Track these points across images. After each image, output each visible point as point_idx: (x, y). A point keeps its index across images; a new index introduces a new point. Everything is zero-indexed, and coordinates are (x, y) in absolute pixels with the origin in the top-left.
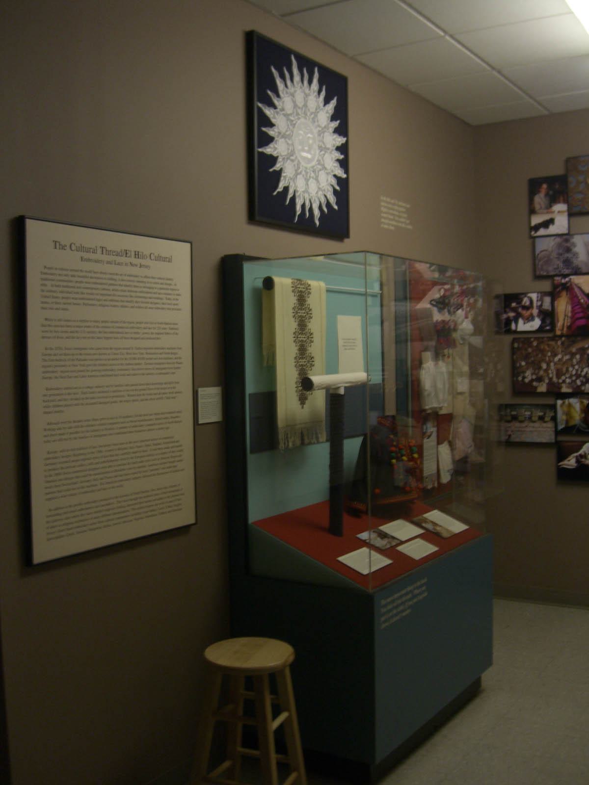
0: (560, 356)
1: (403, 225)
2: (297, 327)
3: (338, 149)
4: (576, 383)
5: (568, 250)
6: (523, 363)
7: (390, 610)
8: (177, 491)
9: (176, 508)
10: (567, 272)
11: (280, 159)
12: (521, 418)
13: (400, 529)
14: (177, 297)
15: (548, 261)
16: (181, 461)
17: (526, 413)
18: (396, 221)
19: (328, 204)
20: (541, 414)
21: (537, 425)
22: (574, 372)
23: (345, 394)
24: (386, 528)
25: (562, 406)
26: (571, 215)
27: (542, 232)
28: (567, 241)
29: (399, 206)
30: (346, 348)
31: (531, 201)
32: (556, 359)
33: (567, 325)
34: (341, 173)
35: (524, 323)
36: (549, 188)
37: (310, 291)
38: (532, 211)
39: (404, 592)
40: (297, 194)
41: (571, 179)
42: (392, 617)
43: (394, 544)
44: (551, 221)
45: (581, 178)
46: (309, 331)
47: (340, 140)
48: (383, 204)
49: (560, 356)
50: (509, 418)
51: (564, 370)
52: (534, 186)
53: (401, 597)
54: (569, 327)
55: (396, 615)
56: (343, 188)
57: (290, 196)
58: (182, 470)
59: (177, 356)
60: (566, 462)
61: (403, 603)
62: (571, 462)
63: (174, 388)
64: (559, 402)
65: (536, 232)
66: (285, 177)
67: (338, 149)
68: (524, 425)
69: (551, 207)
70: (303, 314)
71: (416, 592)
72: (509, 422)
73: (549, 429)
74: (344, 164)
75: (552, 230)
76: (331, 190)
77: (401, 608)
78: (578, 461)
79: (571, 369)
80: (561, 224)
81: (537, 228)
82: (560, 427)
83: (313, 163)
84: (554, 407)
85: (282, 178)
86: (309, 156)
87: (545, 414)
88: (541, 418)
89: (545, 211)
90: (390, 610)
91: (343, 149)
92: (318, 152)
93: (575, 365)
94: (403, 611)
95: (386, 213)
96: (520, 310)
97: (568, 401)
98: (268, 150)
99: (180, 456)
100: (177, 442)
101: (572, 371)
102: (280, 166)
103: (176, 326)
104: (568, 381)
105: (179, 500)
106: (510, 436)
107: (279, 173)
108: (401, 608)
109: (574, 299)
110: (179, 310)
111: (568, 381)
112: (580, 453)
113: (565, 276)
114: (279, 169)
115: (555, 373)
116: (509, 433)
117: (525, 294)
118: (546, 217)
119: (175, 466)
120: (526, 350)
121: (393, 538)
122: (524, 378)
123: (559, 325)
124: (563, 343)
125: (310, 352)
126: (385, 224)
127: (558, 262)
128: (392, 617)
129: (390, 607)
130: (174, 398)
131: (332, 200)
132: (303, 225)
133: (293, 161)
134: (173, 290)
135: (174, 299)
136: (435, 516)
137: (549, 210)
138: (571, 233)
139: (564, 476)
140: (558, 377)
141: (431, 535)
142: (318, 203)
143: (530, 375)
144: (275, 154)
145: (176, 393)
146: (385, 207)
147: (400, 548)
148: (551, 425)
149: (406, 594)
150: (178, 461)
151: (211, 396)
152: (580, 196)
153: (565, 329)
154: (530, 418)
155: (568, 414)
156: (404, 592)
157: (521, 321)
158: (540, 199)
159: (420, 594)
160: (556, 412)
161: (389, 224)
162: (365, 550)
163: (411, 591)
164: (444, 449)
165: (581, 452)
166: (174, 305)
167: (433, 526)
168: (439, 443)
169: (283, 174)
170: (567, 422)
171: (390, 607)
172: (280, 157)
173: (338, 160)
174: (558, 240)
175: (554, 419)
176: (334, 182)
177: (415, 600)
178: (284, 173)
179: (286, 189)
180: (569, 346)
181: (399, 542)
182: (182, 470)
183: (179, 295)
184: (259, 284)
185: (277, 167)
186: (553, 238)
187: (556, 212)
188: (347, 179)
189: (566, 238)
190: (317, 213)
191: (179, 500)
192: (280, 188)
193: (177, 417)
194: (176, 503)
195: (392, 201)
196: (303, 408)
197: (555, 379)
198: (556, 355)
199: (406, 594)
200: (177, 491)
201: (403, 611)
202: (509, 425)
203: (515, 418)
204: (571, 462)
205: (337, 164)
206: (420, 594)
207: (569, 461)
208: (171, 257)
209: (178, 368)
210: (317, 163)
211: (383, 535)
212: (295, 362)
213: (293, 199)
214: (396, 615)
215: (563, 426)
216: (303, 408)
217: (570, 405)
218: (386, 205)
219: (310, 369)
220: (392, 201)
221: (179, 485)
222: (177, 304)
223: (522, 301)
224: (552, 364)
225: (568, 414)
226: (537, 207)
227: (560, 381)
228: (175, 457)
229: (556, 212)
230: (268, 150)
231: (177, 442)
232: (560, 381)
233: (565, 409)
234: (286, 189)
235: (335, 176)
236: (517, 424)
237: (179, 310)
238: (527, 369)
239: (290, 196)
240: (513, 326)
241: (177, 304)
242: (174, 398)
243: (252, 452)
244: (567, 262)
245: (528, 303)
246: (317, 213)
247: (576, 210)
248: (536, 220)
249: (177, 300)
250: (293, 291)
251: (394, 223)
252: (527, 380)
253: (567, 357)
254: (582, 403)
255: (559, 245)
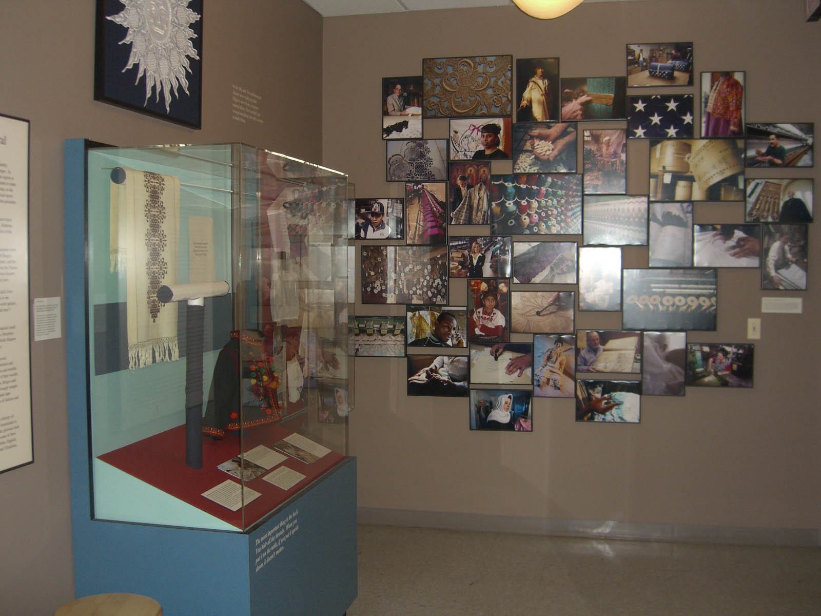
0: (411, 266)
1: (254, 119)
2: (161, 225)
3: (191, 26)
4: (427, 295)
5: (422, 155)
6: (372, 273)
7: (265, 550)
8: (11, 423)
9: (9, 445)
10: (420, 178)
11: (130, 31)
12: (369, 331)
13: (263, 456)
14: (12, 187)
15: (400, 166)
16: (15, 386)
17: (375, 326)
18: (248, 113)
19: (180, 88)
20: (391, 327)
21: (387, 338)
22: (425, 283)
23: (204, 305)
24: (247, 456)
25: (411, 318)
26: (424, 117)
27: (394, 135)
28: (420, 145)
29: (250, 97)
30: (197, 253)
31: (385, 102)
32: (407, 269)
33: (419, 234)
34: (193, 53)
35: (374, 231)
36: (404, 89)
37: (164, 186)
38: (386, 113)
39: (276, 528)
40: (148, 74)
41: (426, 81)
42: (266, 557)
43: (259, 473)
44: (405, 124)
45: (437, 81)
46: (162, 233)
47: (194, 17)
48: (234, 93)
49: (411, 266)
50: (357, 331)
51: (415, 280)
52: (388, 85)
53: (274, 534)
54: (421, 236)
55: (269, 555)
56: (195, 71)
57: (140, 75)
58: (17, 398)
59: (10, 259)
60: (416, 377)
61: (277, 540)
62: (421, 377)
63: (7, 298)
64: (410, 314)
65: (388, 135)
66: (135, 53)
67: (191, 26)
68: (374, 337)
69: (404, 109)
70: (155, 213)
71: (288, 526)
72: (356, 335)
73: (399, 343)
74: (198, 43)
75: (405, 133)
76: (184, 72)
77: (275, 546)
78: (428, 376)
79: (422, 280)
80: (414, 128)
81: (389, 131)
82: (410, 341)
83: (165, 41)
84: (404, 319)
85: (132, 54)
86: (162, 33)
87: (395, 327)
88: (391, 331)
89: (399, 113)
90: (265, 550)
91: (197, 27)
92: (171, 28)
93: (426, 276)
94: (276, 550)
95: (238, 103)
96: (370, 216)
97: (419, 313)
98: (118, 19)
99: (14, 381)
100: (11, 364)
101: (423, 282)
102: (130, 39)
103: (8, 223)
104: (419, 292)
105: (13, 434)
106: (357, 350)
107: (129, 47)
108: (275, 546)
109: (425, 205)
110: (14, 203)
111: (419, 292)
112: (431, 367)
113: (417, 183)
114: (129, 43)
115: (405, 284)
116: (357, 347)
117: (375, 200)
118: (400, 120)
119: (8, 394)
120: (376, 259)
121: (258, 467)
122: (373, 288)
123: (411, 233)
124: (414, 253)
125: (162, 256)
126: (236, 115)
127: (411, 168)
128: (266, 557)
129: (264, 547)
130: (6, 310)
131: (185, 83)
132: (154, 109)
133: (143, 35)
134: (6, 178)
135: (7, 190)
136: (295, 439)
137: (403, 113)
138: (424, 138)
139: (415, 389)
140: (409, 288)
141: (293, 463)
142: (169, 86)
143: (379, 286)
144: (125, 25)
145: (9, 304)
146: (237, 97)
147: (265, 478)
148: (400, 338)
149: (278, 531)
150: (11, 387)
151: (50, 309)
152: (435, 100)
153: (416, 238)
154: (379, 331)
155: (419, 327)
156: (276, 528)
157: (370, 228)
158: (393, 100)
159: (292, 528)
160: (406, 325)
161: (240, 116)
162: (229, 481)
163: (284, 527)
164: (293, 368)
165: (432, 366)
166: (8, 196)
167: (295, 450)
168: (289, 358)
169: (134, 50)
170: (417, 335)
171: (264, 547)
172: (130, 29)
173: (191, 39)
174: (411, 144)
175: (404, 332)
176: (187, 63)
177: (287, 536)
178: (135, 48)
179: (136, 66)
180: (421, 256)
181: (264, 471)
182: (17, 398)
183: (13, 185)
184: (501, 84)
185: (127, 40)
186: (406, 142)
187: (410, 115)
188: (200, 61)
189: (419, 142)
190: (168, 98)
191: (13, 434)
192: (130, 66)
193: (11, 334)
194: (10, 438)
195: (244, 91)
196: (154, 321)
197: (405, 290)
198: (407, 265)
199: (278, 531)
200: (11, 423)
201: (276, 550)
202: (357, 338)
203: (363, 331)
204: (421, 377)
205: (190, 43)
206: (292, 528)
207: (419, 375)
208: (5, 137)
209: (12, 274)
210: (170, 40)
211: (248, 465)
212: (147, 268)
213: (144, 78)
214: (269, 555)
215: (413, 339)
216: (154, 321)
217: (420, 317)
218: (237, 94)
219: (162, 276)
220: (244, 91)
221: (13, 416)
222: (11, 196)
223: (373, 206)
224: (403, 275)
225: (419, 327)
226: (390, 108)
227: (411, 292)
228: (8, 382)
229: (410, 115)
230: (118, 19)
231: (11, 364)
232: (411, 292)
233: (416, 322)
234: (136, 66)
235: (188, 57)
236: (366, 338)
237: (14, 203)
238: (377, 279)
239: (140, 75)
240: (362, 234)
241: (11, 196)
242: (6, 310)
243: (98, 373)
244: (420, 168)
245: (378, 210)
246: (168, 98)
247: (430, 114)
248: (389, 122)
249: (11, 190)
250: (163, 180)
251: (245, 115)
252: (376, 291)
253: (419, 267)
254: (432, 315)
255: (412, 150)
